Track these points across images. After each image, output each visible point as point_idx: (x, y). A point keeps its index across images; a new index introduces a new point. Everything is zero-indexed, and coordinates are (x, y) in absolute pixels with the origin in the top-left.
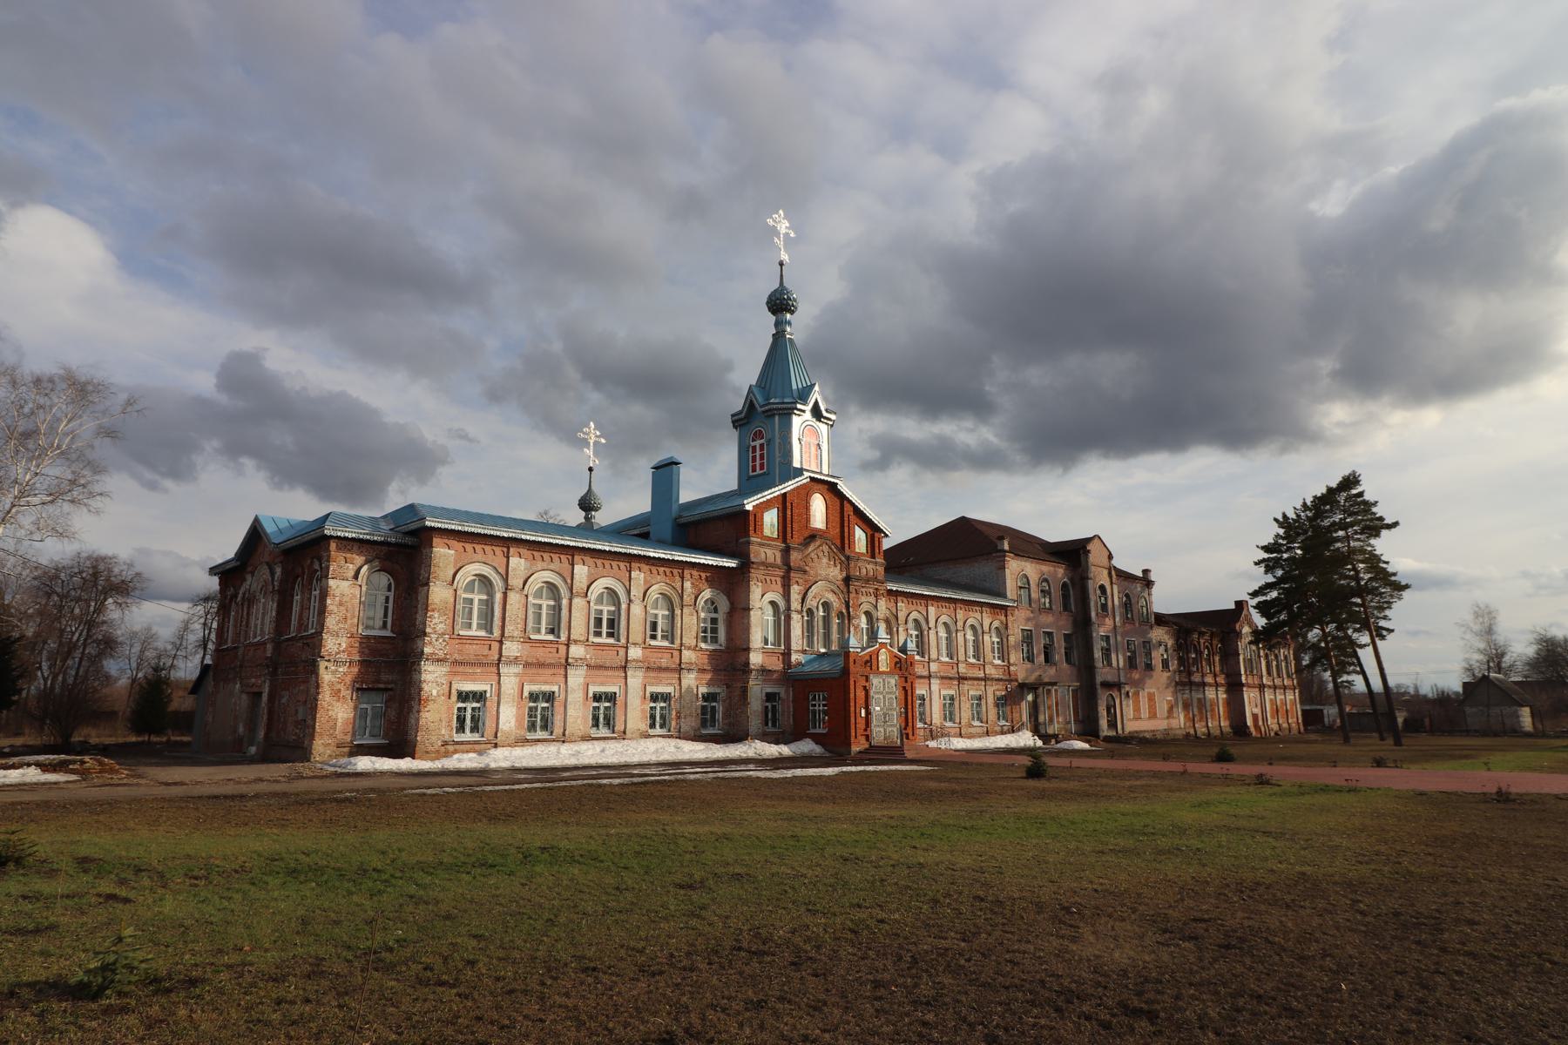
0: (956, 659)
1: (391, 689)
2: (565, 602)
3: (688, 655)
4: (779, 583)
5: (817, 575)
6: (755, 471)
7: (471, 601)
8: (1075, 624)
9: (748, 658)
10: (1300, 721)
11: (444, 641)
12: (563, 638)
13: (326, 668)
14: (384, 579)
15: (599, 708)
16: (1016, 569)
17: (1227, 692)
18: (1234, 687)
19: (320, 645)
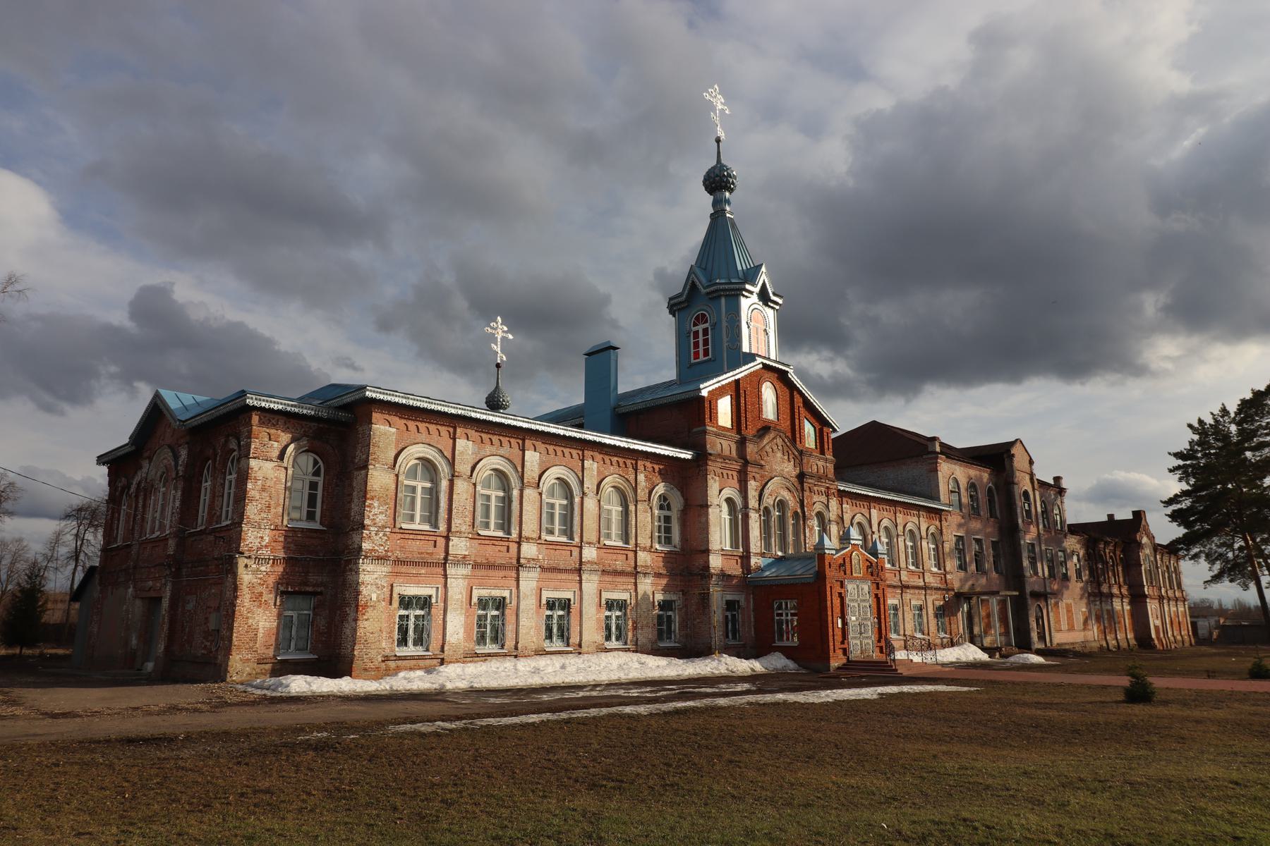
0: (898, 566)
1: (321, 593)
2: (515, 493)
3: (643, 557)
4: (735, 478)
5: (772, 471)
6: (698, 358)
7: (414, 489)
8: (1001, 530)
9: (708, 561)
10: (1191, 633)
11: (384, 535)
12: (514, 535)
13: (246, 566)
14: (307, 461)
15: (611, 617)
16: (946, 469)
17: (1131, 603)
18: (1138, 599)
19: (239, 539)
